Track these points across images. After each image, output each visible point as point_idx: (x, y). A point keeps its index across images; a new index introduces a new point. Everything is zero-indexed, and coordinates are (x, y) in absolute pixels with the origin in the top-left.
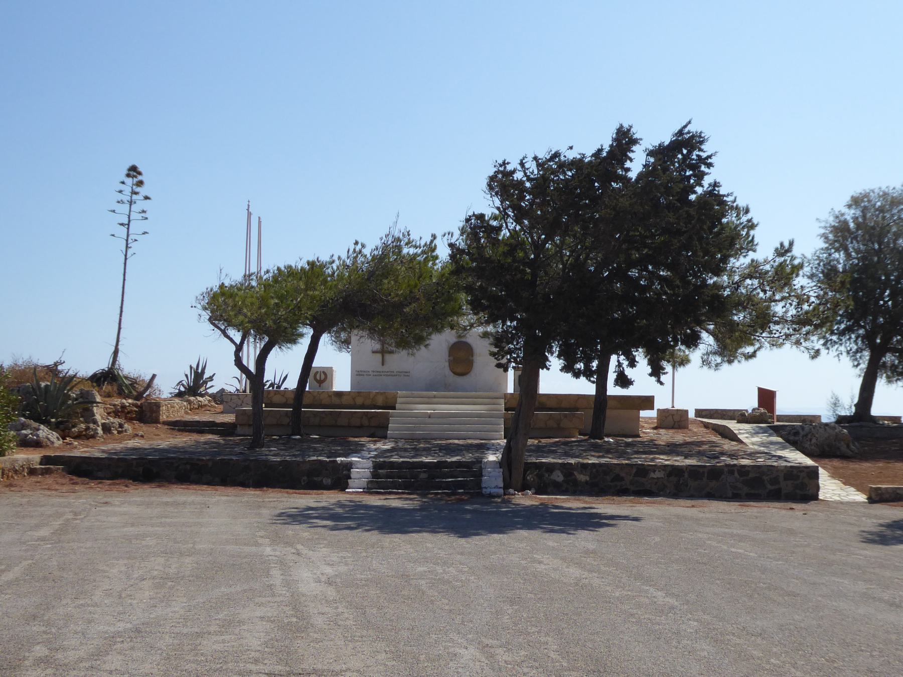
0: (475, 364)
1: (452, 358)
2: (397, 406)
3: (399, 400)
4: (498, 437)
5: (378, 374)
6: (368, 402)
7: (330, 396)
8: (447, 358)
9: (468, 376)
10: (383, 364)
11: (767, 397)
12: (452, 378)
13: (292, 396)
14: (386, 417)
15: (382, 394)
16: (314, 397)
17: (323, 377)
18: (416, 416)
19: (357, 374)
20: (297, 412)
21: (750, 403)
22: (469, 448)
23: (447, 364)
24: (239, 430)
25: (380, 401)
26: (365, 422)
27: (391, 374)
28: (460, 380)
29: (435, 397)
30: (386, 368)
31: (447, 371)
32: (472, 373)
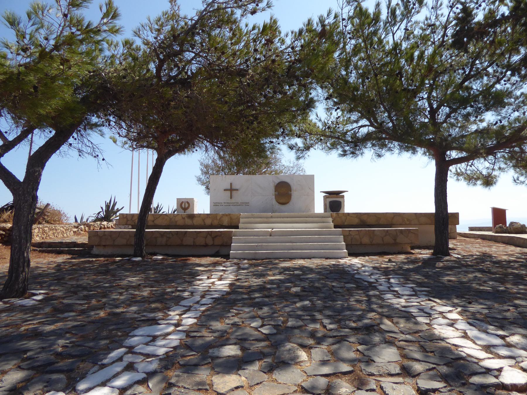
0: (292, 197)
1: (277, 193)
2: (240, 225)
3: (242, 220)
4: (344, 255)
5: (228, 204)
6: (216, 223)
7: (183, 218)
8: (274, 193)
9: (288, 205)
10: (231, 198)
11: (499, 215)
12: (277, 206)
13: (136, 218)
14: (229, 236)
15: (227, 215)
16: (171, 219)
17: (187, 205)
18: (257, 234)
19: (214, 204)
20: (140, 234)
21: (487, 220)
22: (476, 358)
23: (274, 197)
24: (95, 251)
25: (226, 222)
26: (210, 241)
27: (236, 204)
28: (283, 207)
29: (272, 217)
30: (233, 201)
31: (274, 202)
32: (291, 203)
